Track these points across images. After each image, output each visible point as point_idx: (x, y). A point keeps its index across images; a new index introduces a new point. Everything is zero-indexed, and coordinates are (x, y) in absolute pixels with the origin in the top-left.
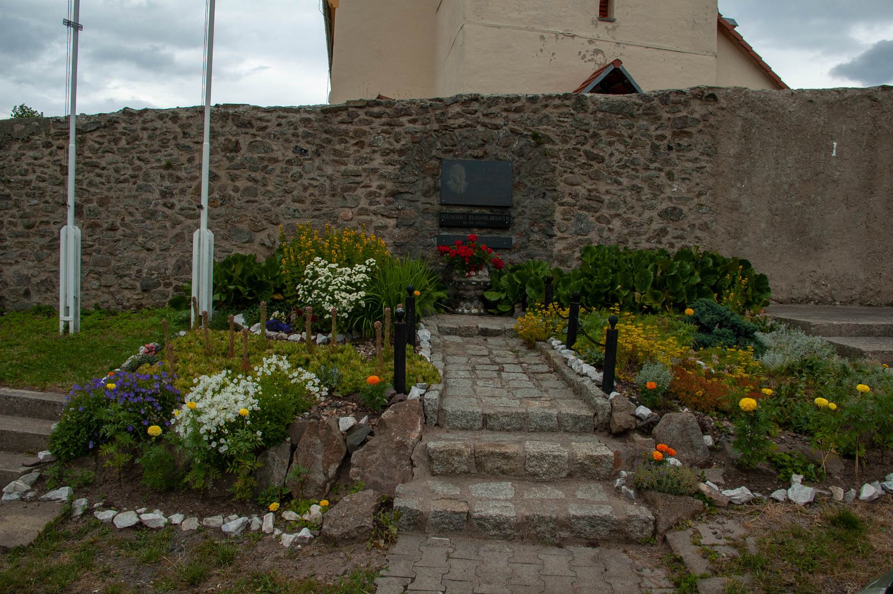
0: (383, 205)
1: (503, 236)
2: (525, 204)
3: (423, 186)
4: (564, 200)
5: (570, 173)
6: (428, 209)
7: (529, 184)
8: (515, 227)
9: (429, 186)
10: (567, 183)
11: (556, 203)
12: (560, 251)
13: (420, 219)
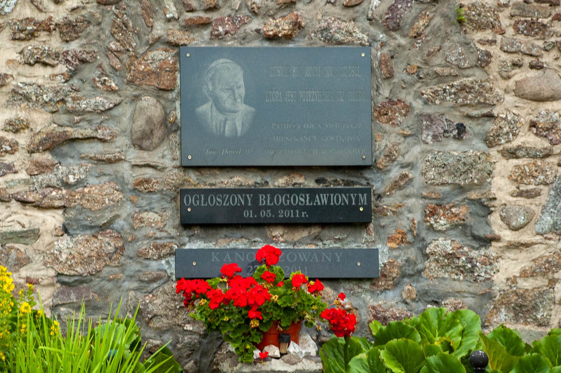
0: (23, 175)
1: (354, 246)
2: (408, 158)
3: (133, 119)
4: (516, 143)
5: (532, 67)
6: (147, 181)
7: (418, 105)
8: (384, 221)
9: (149, 121)
10: (522, 96)
11: (494, 152)
12: (512, 280)
13: (128, 208)
